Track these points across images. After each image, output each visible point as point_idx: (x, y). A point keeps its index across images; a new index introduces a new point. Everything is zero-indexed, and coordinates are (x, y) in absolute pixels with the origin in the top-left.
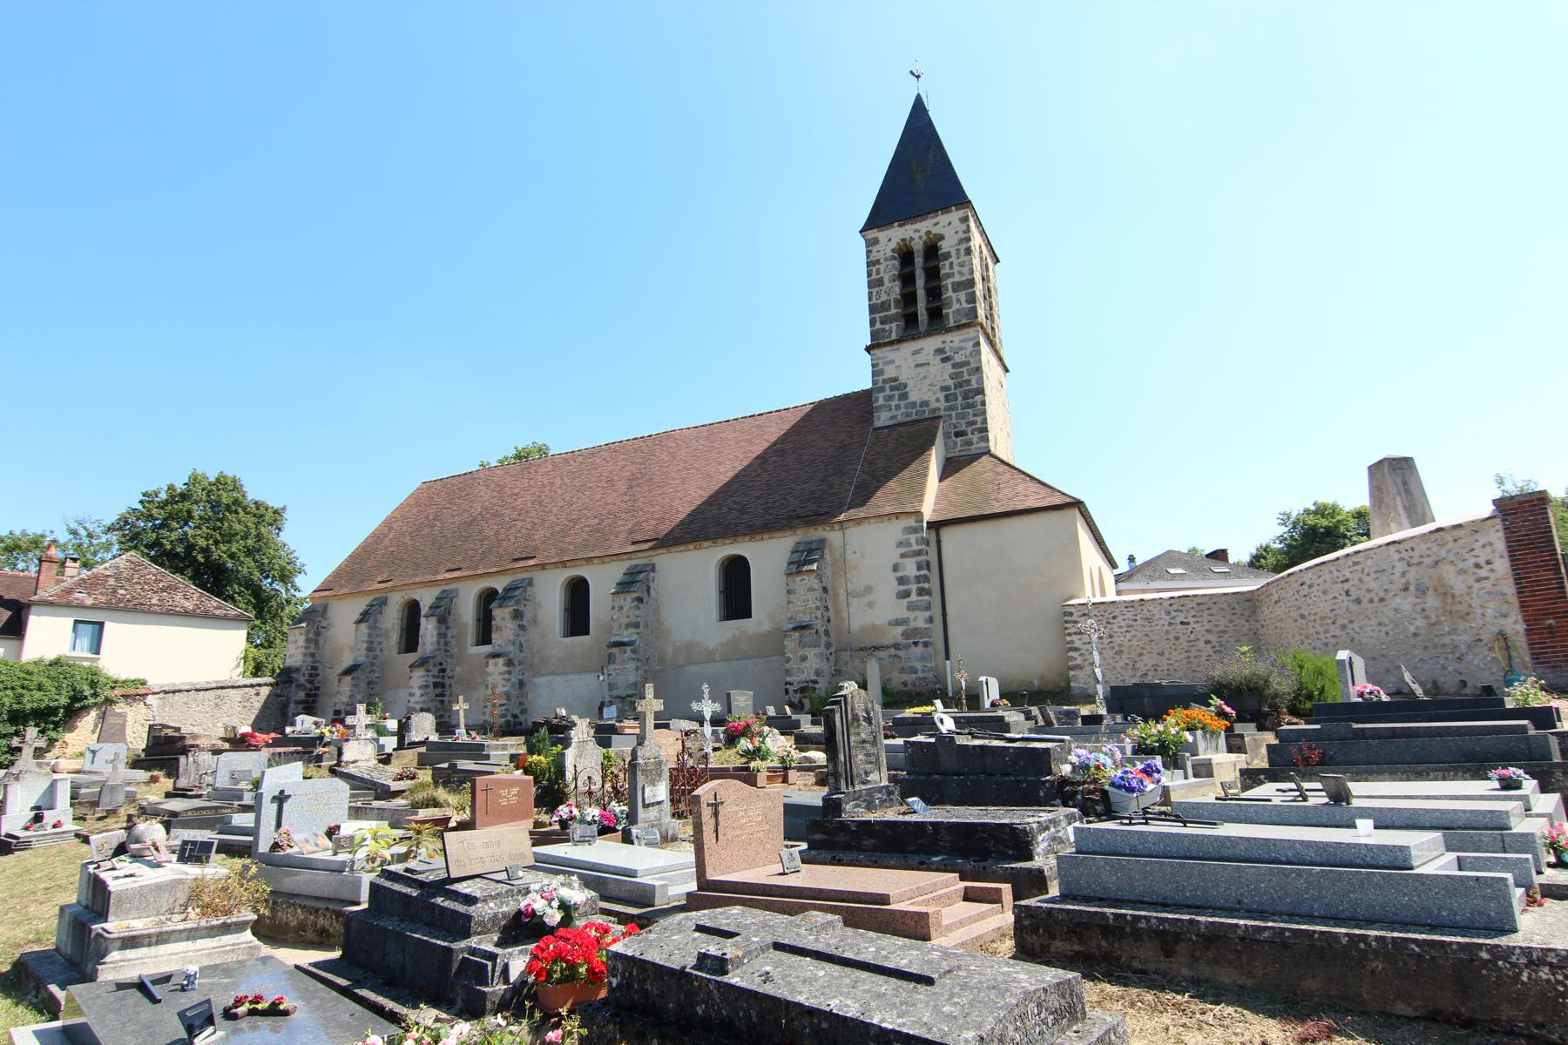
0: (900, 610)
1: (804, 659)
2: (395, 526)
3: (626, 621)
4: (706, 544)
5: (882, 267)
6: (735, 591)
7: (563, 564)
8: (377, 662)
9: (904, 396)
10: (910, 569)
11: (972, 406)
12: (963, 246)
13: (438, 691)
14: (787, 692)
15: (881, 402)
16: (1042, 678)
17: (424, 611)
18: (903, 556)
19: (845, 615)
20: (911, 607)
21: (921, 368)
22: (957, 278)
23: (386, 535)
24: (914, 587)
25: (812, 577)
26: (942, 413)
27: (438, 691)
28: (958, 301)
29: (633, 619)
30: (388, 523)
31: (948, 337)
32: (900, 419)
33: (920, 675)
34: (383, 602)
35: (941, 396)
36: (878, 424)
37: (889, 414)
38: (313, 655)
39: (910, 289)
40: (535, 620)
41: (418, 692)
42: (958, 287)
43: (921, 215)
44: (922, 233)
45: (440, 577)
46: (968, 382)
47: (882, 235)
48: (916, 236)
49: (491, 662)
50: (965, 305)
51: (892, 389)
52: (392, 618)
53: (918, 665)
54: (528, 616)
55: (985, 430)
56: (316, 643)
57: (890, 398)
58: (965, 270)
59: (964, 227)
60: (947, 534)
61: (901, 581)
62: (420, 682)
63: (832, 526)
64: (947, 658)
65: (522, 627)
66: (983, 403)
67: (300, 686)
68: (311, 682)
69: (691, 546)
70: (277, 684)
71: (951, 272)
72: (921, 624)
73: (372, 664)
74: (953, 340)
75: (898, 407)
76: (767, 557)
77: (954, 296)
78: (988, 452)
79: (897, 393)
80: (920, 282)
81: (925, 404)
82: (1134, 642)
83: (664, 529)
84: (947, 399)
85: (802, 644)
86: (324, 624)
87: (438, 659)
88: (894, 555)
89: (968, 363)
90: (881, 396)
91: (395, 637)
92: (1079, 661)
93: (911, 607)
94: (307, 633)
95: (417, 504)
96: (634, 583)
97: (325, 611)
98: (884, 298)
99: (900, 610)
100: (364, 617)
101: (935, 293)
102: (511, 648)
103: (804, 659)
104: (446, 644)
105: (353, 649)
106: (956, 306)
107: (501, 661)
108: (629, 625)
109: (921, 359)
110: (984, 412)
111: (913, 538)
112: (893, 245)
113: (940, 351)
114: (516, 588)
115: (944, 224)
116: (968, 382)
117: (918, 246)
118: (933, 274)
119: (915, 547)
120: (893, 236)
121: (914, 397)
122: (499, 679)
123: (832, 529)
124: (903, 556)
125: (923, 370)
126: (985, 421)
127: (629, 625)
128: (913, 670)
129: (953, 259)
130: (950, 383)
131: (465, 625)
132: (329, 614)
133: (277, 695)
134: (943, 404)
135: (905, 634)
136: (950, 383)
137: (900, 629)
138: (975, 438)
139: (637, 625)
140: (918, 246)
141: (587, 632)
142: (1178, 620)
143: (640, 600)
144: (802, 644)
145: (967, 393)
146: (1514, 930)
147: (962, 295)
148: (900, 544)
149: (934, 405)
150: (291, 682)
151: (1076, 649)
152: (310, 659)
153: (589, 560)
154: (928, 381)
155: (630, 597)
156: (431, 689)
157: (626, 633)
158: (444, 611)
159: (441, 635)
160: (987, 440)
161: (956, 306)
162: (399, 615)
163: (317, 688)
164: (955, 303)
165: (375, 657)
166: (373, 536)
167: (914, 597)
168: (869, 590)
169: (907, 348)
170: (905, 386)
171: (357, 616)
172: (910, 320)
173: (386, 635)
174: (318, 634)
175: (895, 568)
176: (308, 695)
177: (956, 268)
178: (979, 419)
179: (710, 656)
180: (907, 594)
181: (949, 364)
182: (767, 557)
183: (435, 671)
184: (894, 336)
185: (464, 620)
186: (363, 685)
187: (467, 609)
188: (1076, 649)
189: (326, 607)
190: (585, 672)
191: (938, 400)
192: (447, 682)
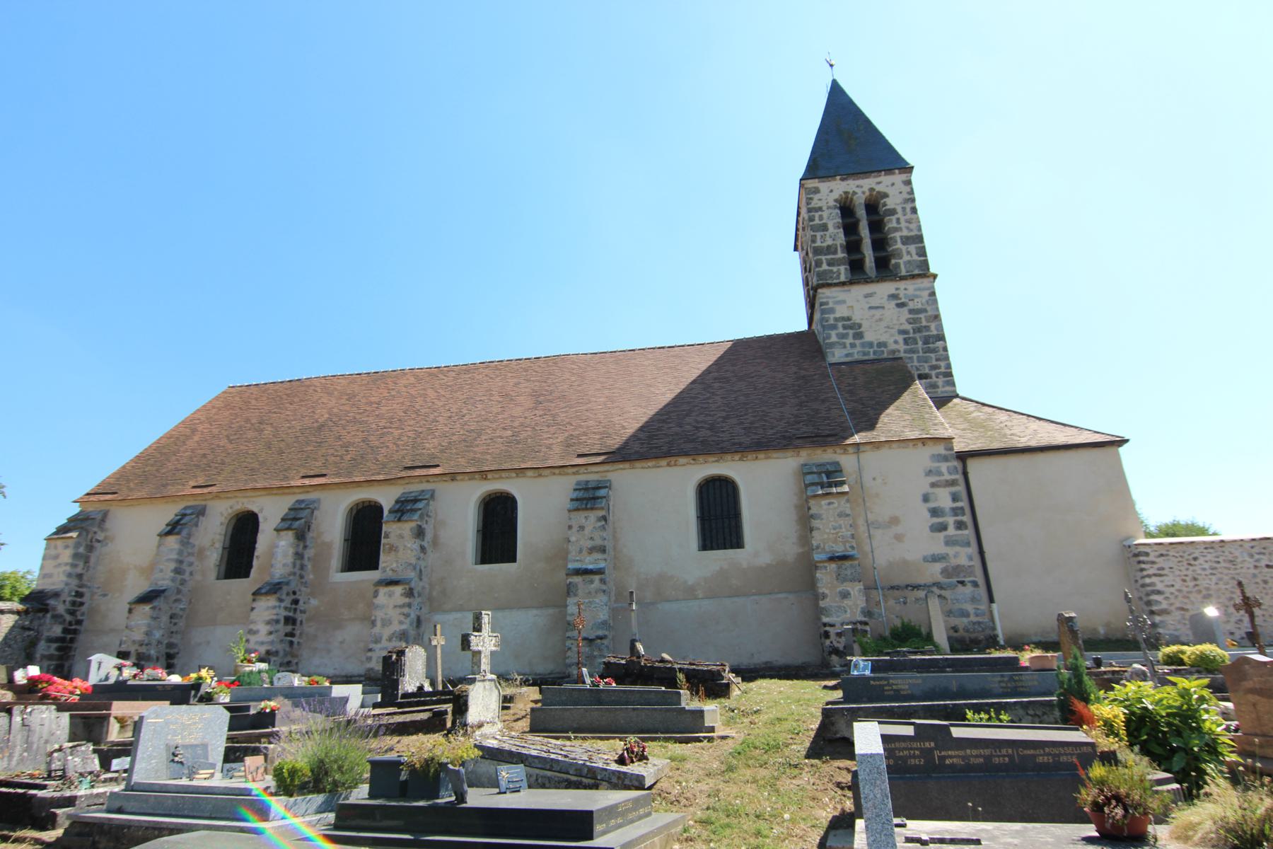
0: (936, 545)
1: (845, 595)
2: (200, 428)
3: (590, 544)
4: (682, 460)
5: (825, 214)
6: (719, 517)
7: (484, 475)
8: (184, 589)
9: (859, 336)
10: (943, 499)
11: (934, 351)
12: (908, 206)
13: (289, 628)
14: (827, 635)
15: (834, 339)
16: (1107, 625)
17: (386, 513)
18: (933, 485)
19: (867, 548)
20: (949, 542)
21: (870, 311)
22: (905, 233)
23: (188, 437)
24: (951, 520)
25: (843, 500)
26: (902, 355)
27: (289, 628)
28: (908, 253)
29: (598, 542)
30: (190, 426)
31: (902, 285)
32: (856, 357)
33: (973, 618)
34: (201, 512)
35: (900, 338)
36: (831, 359)
37: (845, 352)
38: (80, 576)
39: (853, 238)
40: (435, 542)
41: (263, 629)
42: (907, 240)
43: (865, 173)
44: (866, 189)
45: (293, 483)
46: (927, 328)
47: (824, 186)
48: (859, 191)
49: (383, 591)
50: (916, 257)
51: (845, 327)
52: (212, 534)
53: (969, 607)
54: (429, 536)
55: (950, 375)
56: (87, 561)
57: (844, 336)
58: (913, 226)
59: (907, 189)
60: (973, 465)
61: (935, 512)
62: (268, 615)
63: (845, 449)
64: (991, 600)
65: (423, 549)
66: (945, 349)
67: (56, 617)
68: (72, 613)
69: (664, 462)
70: (26, 612)
71: (896, 227)
72: (963, 561)
73: (179, 591)
74: (906, 288)
75: (853, 346)
76: (764, 484)
77: (904, 248)
78: (957, 396)
79: (851, 332)
80: (864, 231)
81: (881, 345)
82: (1222, 586)
83: (615, 442)
84: (906, 341)
85: (840, 578)
86: (100, 536)
87: (293, 586)
88: (924, 485)
89: (925, 311)
90: (833, 333)
91: (214, 557)
92: (1164, 605)
93: (949, 542)
94: (77, 545)
95: (228, 406)
96: (589, 498)
97: (103, 520)
98: (829, 242)
99: (936, 545)
100: (173, 528)
101: (880, 244)
102: (412, 574)
103: (845, 595)
104: (302, 567)
105: (152, 567)
106: (906, 258)
107: (398, 590)
108: (592, 550)
109: (874, 302)
110: (947, 358)
111: (944, 467)
112: (836, 195)
113: (894, 297)
114: (416, 501)
115: (885, 183)
116: (927, 328)
117: (860, 200)
118: (877, 226)
119: (948, 477)
120: (832, 191)
121: (869, 337)
122: (394, 615)
123: (845, 452)
124: (933, 485)
125: (878, 313)
126: (949, 366)
127: (592, 550)
128: (965, 614)
129: (900, 215)
130: (908, 327)
131: (329, 546)
132: (108, 525)
133: (24, 628)
134: (902, 347)
135: (944, 572)
136: (908, 327)
137: (938, 567)
138: (940, 381)
139: (603, 550)
140: (860, 200)
141: (512, 558)
142: (1263, 563)
143: (604, 518)
144: (840, 578)
145: (927, 335)
146: (205, 746)
147: (912, 248)
148: (929, 473)
149: (892, 347)
150: (45, 610)
151: (1159, 592)
152: (75, 582)
153: (520, 471)
154: (883, 324)
155: (593, 516)
156: (281, 626)
157: (588, 559)
158: (299, 523)
159: (299, 556)
160: (954, 385)
161: (906, 258)
162: (222, 530)
163: (79, 622)
164: (904, 258)
165: (183, 582)
166: (169, 436)
167: (951, 531)
168: (895, 521)
169: (859, 291)
170: (860, 326)
171: (162, 526)
172: (856, 266)
173: (201, 553)
174: (90, 548)
175: (926, 499)
176: (65, 631)
177: (903, 224)
178: (942, 364)
179: (690, 593)
180: (943, 528)
181: (905, 310)
182: (764, 484)
183: (287, 603)
184: (843, 278)
185: (327, 538)
186: (165, 619)
187: (332, 527)
188: (1159, 592)
189: (105, 515)
190: (511, 608)
191: (896, 342)
192: (299, 617)
